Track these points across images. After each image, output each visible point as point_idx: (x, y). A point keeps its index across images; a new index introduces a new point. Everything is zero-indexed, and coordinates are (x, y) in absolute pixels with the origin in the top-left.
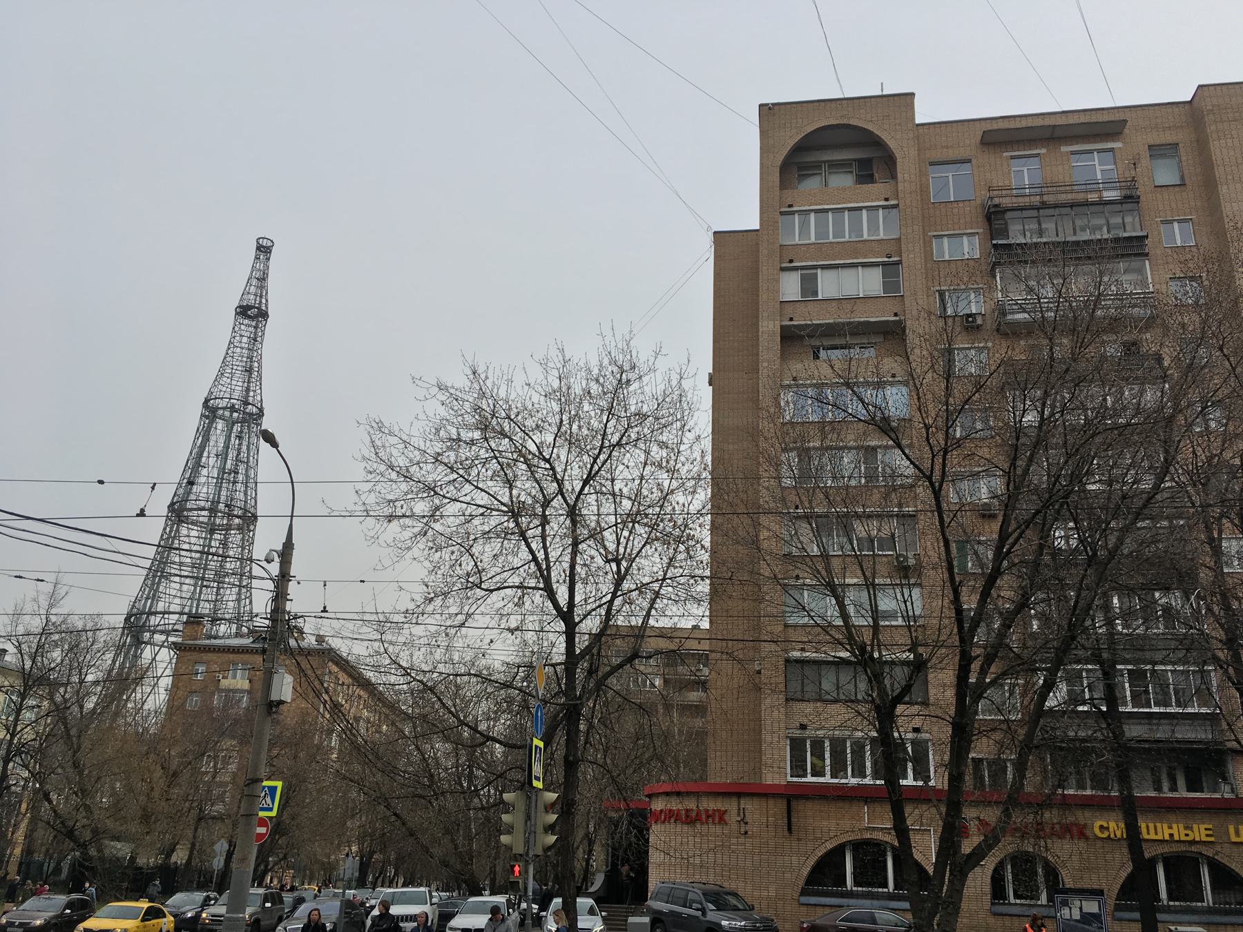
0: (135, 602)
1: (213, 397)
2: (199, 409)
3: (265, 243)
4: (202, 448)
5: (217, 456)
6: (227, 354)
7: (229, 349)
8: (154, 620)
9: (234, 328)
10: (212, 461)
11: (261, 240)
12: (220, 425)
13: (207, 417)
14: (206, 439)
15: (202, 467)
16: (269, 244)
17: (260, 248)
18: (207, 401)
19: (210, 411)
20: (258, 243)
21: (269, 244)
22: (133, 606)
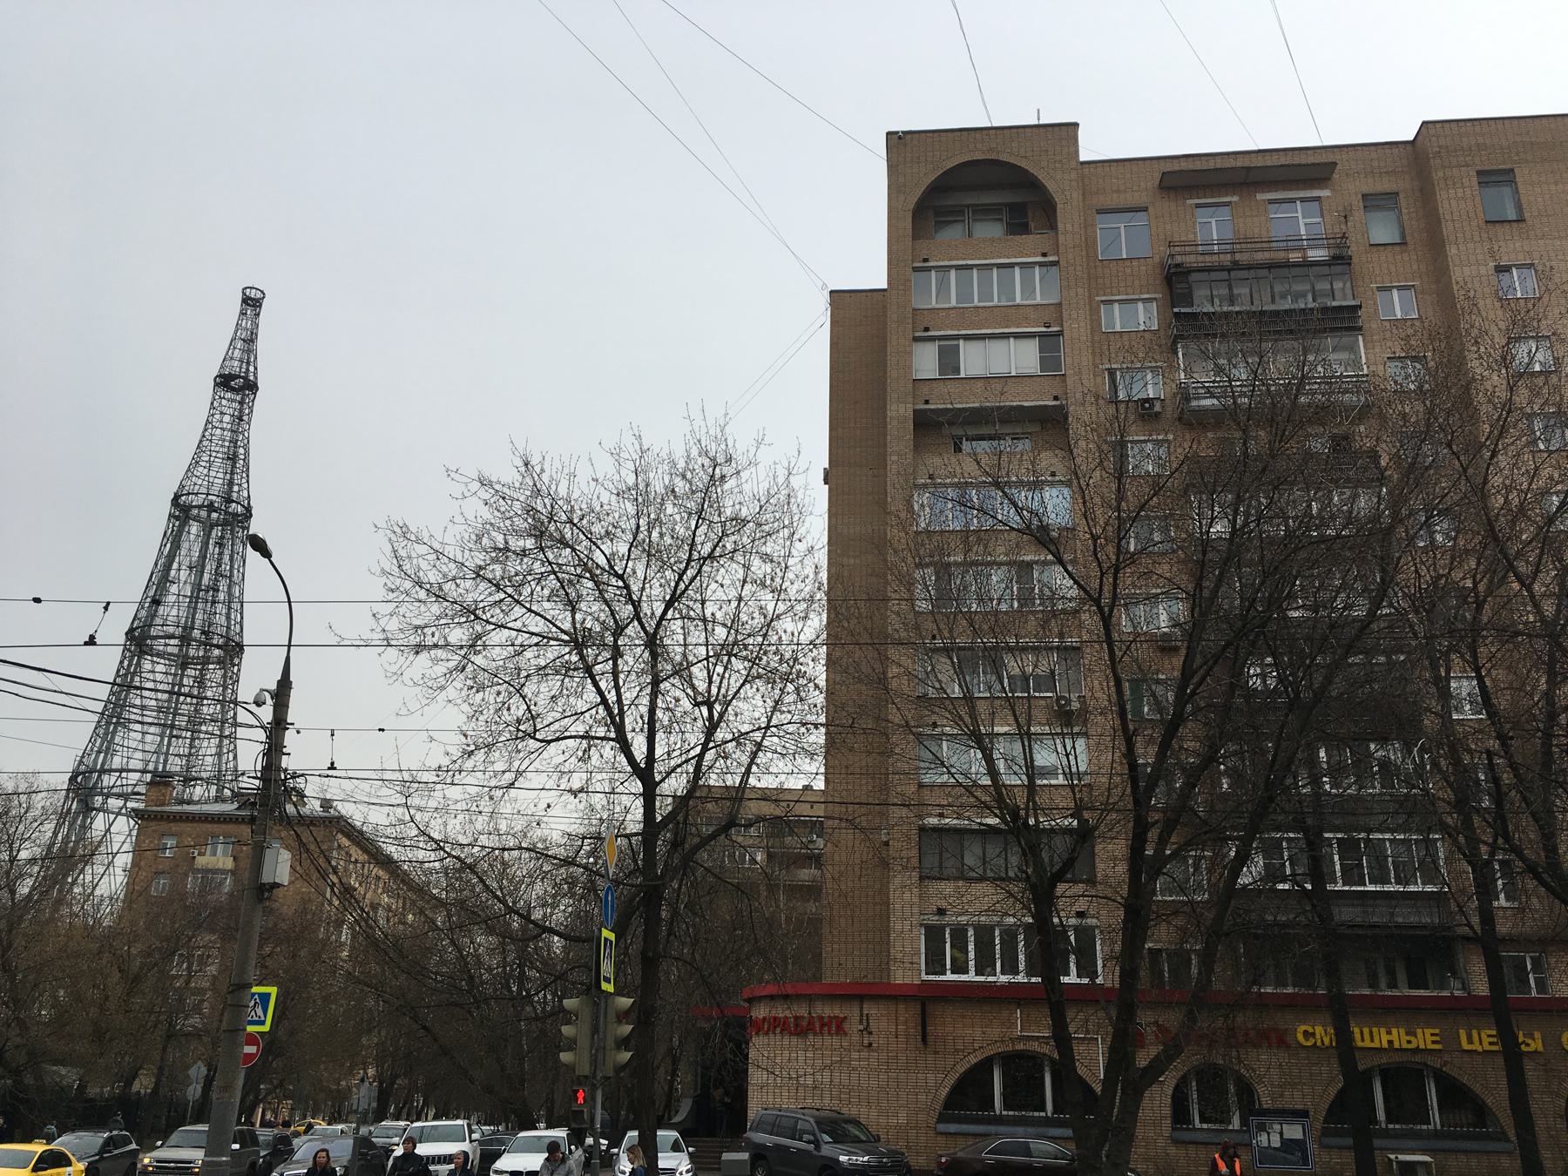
0: (83, 757)
1: (185, 492)
2: (166, 507)
3: (253, 294)
4: (171, 558)
5: (191, 568)
6: (204, 436)
7: (206, 430)
8: (108, 780)
9: (212, 403)
10: (184, 574)
11: (248, 290)
12: (194, 528)
13: (177, 518)
14: (176, 546)
15: (171, 582)
16: (259, 295)
17: (246, 300)
18: (176, 497)
19: (181, 511)
20: (244, 294)
21: (258, 296)
22: (81, 762)
